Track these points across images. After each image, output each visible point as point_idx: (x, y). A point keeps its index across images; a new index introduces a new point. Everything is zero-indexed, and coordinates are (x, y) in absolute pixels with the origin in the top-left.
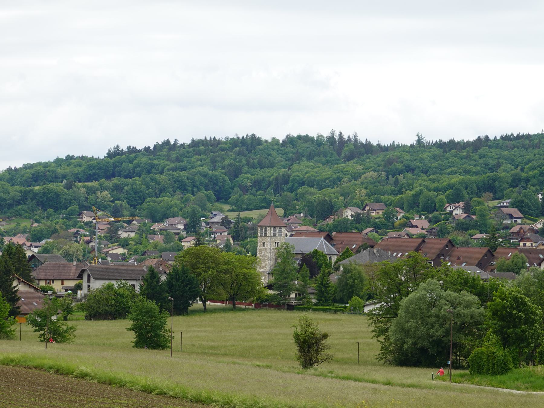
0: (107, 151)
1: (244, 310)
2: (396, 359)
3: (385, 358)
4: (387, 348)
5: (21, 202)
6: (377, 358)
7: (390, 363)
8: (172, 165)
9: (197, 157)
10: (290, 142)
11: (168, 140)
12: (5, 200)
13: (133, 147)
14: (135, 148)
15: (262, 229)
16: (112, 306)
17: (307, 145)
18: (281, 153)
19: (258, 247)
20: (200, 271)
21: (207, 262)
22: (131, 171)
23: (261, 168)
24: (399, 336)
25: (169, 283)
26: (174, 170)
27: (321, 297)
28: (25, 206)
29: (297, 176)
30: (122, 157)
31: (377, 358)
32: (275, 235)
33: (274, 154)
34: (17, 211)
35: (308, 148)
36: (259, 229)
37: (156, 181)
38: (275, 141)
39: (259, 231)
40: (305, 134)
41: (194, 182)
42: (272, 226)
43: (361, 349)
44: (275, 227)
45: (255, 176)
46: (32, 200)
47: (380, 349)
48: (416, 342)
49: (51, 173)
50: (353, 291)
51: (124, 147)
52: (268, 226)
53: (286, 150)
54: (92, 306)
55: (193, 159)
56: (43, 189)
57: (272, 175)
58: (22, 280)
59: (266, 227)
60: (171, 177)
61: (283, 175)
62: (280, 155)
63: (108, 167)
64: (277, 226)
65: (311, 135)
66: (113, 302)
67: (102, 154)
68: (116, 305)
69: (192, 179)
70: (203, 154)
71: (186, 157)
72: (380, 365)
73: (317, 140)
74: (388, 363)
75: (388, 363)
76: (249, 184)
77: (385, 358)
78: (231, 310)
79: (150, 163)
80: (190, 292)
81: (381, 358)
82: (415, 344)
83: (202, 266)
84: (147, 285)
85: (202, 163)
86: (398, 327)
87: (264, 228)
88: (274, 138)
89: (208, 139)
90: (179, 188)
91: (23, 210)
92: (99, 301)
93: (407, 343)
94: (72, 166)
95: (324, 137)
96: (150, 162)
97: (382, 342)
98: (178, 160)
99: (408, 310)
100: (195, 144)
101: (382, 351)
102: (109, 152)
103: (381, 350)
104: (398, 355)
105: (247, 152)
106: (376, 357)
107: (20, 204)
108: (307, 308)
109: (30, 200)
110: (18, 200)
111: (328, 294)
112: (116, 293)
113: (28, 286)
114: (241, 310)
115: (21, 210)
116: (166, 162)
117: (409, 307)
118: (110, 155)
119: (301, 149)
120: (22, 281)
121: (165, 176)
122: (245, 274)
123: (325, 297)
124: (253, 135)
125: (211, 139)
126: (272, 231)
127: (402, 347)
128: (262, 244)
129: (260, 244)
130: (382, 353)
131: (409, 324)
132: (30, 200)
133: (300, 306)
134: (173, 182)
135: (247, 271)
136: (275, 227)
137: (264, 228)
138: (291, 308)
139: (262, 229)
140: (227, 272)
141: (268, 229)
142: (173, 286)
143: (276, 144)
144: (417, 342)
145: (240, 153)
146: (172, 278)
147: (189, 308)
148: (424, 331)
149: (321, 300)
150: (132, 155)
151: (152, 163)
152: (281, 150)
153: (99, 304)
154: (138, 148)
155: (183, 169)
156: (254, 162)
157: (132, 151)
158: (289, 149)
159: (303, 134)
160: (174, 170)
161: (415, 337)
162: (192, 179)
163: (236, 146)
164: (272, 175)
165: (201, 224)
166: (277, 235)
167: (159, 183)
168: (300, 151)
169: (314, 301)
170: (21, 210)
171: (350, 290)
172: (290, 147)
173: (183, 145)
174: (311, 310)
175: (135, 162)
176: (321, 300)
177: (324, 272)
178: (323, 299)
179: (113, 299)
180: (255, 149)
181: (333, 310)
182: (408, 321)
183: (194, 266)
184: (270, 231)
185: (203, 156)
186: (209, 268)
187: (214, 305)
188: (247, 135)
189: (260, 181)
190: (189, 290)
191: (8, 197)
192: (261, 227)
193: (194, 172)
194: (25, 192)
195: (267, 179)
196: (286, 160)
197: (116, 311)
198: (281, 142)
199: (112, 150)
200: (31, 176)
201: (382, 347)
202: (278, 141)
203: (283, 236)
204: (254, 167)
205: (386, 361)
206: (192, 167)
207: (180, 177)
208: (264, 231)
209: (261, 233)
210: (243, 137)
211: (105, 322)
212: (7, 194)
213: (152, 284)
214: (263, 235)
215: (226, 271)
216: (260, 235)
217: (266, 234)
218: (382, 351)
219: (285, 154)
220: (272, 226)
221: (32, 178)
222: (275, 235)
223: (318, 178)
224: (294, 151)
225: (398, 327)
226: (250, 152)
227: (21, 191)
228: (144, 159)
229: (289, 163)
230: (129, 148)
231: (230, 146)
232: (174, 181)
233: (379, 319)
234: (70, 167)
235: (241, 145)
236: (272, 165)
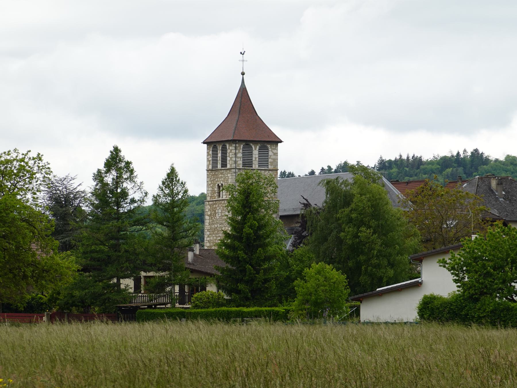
32: (248, 163)
42: (240, 141)
44: (247, 144)
50: (359, 265)
64: (255, 142)
87: (220, 148)
88: (508, 156)
89: (404, 157)
124: (476, 150)
125: (408, 157)
126: (240, 155)
137: (220, 148)
141: (231, 149)
163: (447, 167)
171: (350, 264)
178: (241, 286)
188: (465, 151)
208: (220, 155)
214: (219, 166)
215: (172, 316)
217: (224, 165)
220: (240, 141)
231: (438, 166)
235: (456, 165)
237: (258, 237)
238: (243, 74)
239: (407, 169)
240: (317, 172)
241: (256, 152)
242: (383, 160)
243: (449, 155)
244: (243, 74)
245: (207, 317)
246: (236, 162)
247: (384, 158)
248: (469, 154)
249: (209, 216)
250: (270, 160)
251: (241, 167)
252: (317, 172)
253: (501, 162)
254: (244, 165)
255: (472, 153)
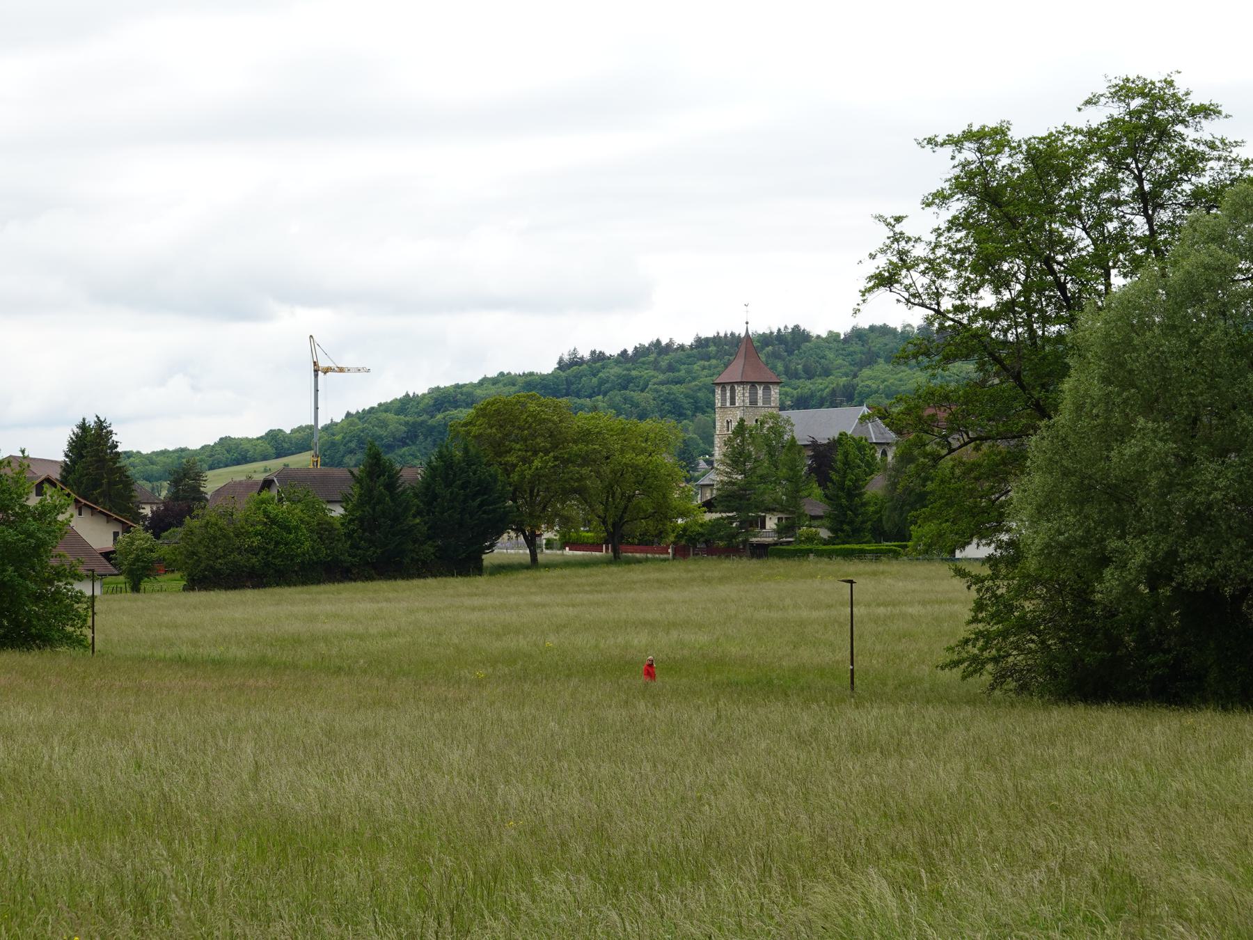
0: (557, 360)
1: (639, 561)
2: (1057, 666)
3: (995, 660)
4: (1002, 610)
5: (407, 441)
6: (956, 664)
7: (1023, 688)
8: (661, 377)
9: (702, 363)
10: (857, 337)
11: (658, 341)
12: (380, 438)
13: (600, 352)
14: (603, 354)
15: (724, 390)
16: (253, 551)
17: (886, 340)
18: (842, 355)
19: (718, 432)
20: (511, 459)
21: (533, 436)
22: (596, 390)
23: (809, 379)
24: (1069, 523)
25: (428, 493)
26: (662, 383)
27: (842, 523)
28: (414, 448)
29: (867, 386)
30: (581, 368)
31: (956, 664)
32: (753, 402)
33: (831, 355)
34: (401, 457)
35: (886, 345)
36: (718, 391)
37: (632, 401)
38: (833, 337)
39: (718, 396)
40: (881, 324)
41: (696, 402)
42: (747, 383)
43: (858, 604)
44: (753, 385)
45: (799, 390)
46: (426, 438)
47: (968, 615)
48: (1172, 554)
49: (464, 397)
51: (585, 353)
52: (736, 383)
53: (851, 349)
54: (194, 553)
55: (696, 367)
56: (444, 418)
57: (827, 387)
58: (83, 501)
59: (732, 384)
60: (655, 395)
61: (844, 386)
62: (841, 357)
63: (558, 386)
64: (760, 383)
65: (892, 325)
66: (256, 541)
67: (546, 366)
68: (265, 549)
69: (693, 398)
70: (714, 358)
71: (684, 364)
72: (972, 701)
73: (902, 332)
74: (1012, 684)
75: (1012, 684)
76: (789, 403)
77: (995, 660)
78: (609, 562)
79: (624, 375)
80: (484, 512)
81: (974, 659)
82: (1156, 575)
83: (518, 446)
84: (361, 495)
85: (711, 372)
86: (1066, 473)
87: (728, 388)
88: (830, 331)
89: (722, 334)
90: (670, 412)
91: (411, 455)
92: (215, 538)
93: (1123, 566)
94: (500, 385)
95: (913, 328)
96: (625, 372)
97: (979, 580)
98: (671, 368)
99: (1122, 365)
100: (701, 343)
101: (981, 626)
102: (561, 361)
103: (975, 620)
104: (1063, 641)
105: (786, 354)
106: (950, 656)
107: (405, 444)
108: (801, 551)
109: (421, 437)
110: (403, 438)
111: (856, 515)
112: (268, 517)
113: (105, 518)
114: (629, 562)
115: (407, 453)
116: (652, 373)
117: (1128, 342)
118: (562, 366)
119: (874, 346)
120: (85, 505)
121: (648, 392)
122: (635, 467)
123: (851, 523)
124: (797, 327)
125: (726, 335)
126: (747, 395)
127: (1083, 597)
128: (725, 424)
129: (722, 426)
130: (979, 634)
131: (1131, 448)
132: (421, 437)
133: (784, 547)
134: (660, 403)
135: (641, 459)
136: (753, 385)
137: (728, 388)
138: (761, 551)
139: (724, 390)
140: (586, 460)
141: (738, 389)
142: (435, 497)
143: (835, 340)
144: (1183, 554)
145: (776, 355)
146: (433, 477)
147: (484, 556)
148: (1222, 483)
149: (842, 531)
150: (599, 364)
151: (629, 375)
152: (843, 349)
153: (216, 546)
154: (607, 354)
155: (678, 382)
156: (796, 369)
157: (598, 357)
158: (856, 347)
159: (878, 323)
160: (662, 383)
161: (1164, 528)
162: (693, 398)
164: (827, 387)
165: (698, 464)
166: (760, 403)
167: (637, 405)
168: (873, 349)
169: (824, 534)
170: (407, 453)
172: (857, 344)
173: (682, 347)
174: (811, 556)
175: (601, 374)
176: (842, 531)
177: (846, 457)
178: (846, 527)
179: (256, 534)
180: (799, 348)
181: (870, 552)
182: (1123, 434)
183: (499, 449)
184: (742, 395)
185: (714, 362)
186: (535, 453)
187: (583, 555)
188: (786, 327)
189: (807, 398)
190: (480, 506)
191: (385, 434)
192: (723, 385)
193: (696, 385)
194: (414, 425)
195: (818, 394)
196: (851, 364)
197: (267, 564)
198: (842, 337)
199: (566, 358)
200: (431, 402)
201: (980, 606)
202: (838, 335)
203: (772, 405)
204: (796, 376)
205: (999, 679)
206: (694, 379)
207: (673, 394)
208: (728, 394)
209: (724, 400)
210: (779, 330)
211: (250, 594)
212: (384, 429)
213: (375, 493)
214: (728, 404)
215: (583, 459)
216: (719, 405)
217: (733, 403)
218: (981, 626)
219: (849, 355)
220: (747, 383)
221: (434, 405)
222: (753, 402)
223: (903, 388)
224: (865, 349)
225: (1066, 473)
226: (790, 353)
227: (407, 423)
228: (617, 370)
229: (855, 369)
230: (593, 353)
232: (662, 400)
233: (955, 444)
234: (497, 386)
236: (827, 373)
237: (857, 488)
238: (747, 323)
239: (727, 347)
240: (630, 352)
241: (760, 392)
242: (700, 338)
243: (768, 332)
244: (747, 323)
245: (820, 554)
246: (743, 401)
247: (700, 336)
248: (790, 330)
249: (719, 447)
250: (772, 399)
251: (748, 405)
252: (630, 352)
253: (822, 339)
254: (751, 403)
255: (793, 329)
